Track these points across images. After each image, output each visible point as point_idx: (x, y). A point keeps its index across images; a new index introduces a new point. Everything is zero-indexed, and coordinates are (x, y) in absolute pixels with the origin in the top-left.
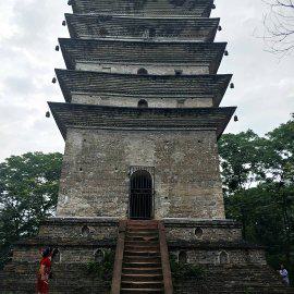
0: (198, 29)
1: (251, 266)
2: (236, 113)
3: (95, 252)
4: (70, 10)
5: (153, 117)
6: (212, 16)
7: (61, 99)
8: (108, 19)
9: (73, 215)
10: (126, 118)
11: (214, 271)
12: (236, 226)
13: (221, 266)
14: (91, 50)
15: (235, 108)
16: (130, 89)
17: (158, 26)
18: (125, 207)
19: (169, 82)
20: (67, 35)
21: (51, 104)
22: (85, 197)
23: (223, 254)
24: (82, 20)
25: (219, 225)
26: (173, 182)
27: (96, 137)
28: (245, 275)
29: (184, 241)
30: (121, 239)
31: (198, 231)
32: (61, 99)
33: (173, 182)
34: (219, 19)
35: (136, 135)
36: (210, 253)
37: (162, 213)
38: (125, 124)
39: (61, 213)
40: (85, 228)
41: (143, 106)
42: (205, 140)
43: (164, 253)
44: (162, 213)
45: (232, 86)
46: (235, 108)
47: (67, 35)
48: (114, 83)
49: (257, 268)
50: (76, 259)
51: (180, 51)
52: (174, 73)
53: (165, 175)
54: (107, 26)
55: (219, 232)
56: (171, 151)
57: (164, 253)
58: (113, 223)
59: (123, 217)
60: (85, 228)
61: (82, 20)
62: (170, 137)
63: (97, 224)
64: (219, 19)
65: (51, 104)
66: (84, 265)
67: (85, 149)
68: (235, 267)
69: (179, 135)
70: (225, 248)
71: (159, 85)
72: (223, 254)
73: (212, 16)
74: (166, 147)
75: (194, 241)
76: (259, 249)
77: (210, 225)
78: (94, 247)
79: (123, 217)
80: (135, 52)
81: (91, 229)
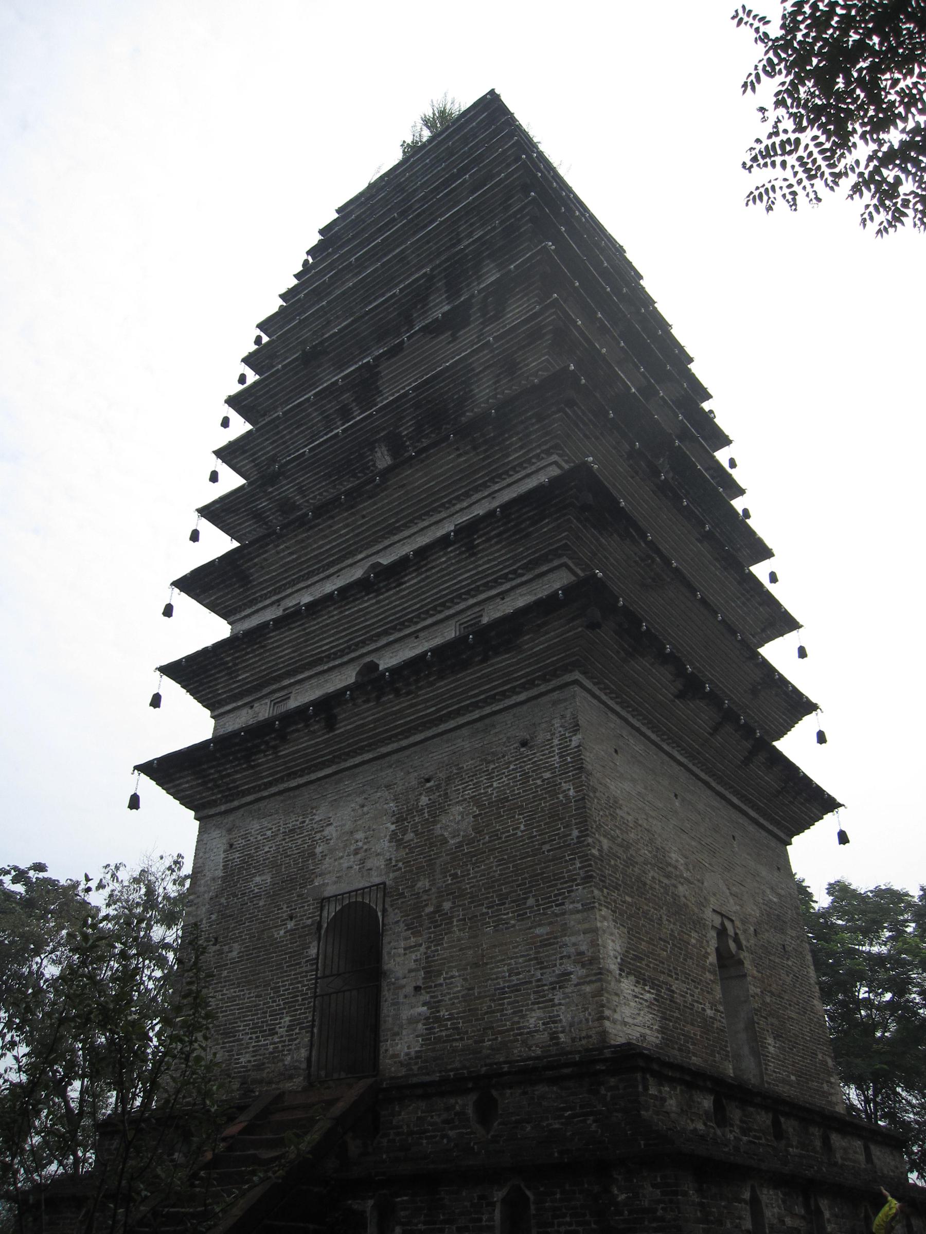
19: (412, 581)
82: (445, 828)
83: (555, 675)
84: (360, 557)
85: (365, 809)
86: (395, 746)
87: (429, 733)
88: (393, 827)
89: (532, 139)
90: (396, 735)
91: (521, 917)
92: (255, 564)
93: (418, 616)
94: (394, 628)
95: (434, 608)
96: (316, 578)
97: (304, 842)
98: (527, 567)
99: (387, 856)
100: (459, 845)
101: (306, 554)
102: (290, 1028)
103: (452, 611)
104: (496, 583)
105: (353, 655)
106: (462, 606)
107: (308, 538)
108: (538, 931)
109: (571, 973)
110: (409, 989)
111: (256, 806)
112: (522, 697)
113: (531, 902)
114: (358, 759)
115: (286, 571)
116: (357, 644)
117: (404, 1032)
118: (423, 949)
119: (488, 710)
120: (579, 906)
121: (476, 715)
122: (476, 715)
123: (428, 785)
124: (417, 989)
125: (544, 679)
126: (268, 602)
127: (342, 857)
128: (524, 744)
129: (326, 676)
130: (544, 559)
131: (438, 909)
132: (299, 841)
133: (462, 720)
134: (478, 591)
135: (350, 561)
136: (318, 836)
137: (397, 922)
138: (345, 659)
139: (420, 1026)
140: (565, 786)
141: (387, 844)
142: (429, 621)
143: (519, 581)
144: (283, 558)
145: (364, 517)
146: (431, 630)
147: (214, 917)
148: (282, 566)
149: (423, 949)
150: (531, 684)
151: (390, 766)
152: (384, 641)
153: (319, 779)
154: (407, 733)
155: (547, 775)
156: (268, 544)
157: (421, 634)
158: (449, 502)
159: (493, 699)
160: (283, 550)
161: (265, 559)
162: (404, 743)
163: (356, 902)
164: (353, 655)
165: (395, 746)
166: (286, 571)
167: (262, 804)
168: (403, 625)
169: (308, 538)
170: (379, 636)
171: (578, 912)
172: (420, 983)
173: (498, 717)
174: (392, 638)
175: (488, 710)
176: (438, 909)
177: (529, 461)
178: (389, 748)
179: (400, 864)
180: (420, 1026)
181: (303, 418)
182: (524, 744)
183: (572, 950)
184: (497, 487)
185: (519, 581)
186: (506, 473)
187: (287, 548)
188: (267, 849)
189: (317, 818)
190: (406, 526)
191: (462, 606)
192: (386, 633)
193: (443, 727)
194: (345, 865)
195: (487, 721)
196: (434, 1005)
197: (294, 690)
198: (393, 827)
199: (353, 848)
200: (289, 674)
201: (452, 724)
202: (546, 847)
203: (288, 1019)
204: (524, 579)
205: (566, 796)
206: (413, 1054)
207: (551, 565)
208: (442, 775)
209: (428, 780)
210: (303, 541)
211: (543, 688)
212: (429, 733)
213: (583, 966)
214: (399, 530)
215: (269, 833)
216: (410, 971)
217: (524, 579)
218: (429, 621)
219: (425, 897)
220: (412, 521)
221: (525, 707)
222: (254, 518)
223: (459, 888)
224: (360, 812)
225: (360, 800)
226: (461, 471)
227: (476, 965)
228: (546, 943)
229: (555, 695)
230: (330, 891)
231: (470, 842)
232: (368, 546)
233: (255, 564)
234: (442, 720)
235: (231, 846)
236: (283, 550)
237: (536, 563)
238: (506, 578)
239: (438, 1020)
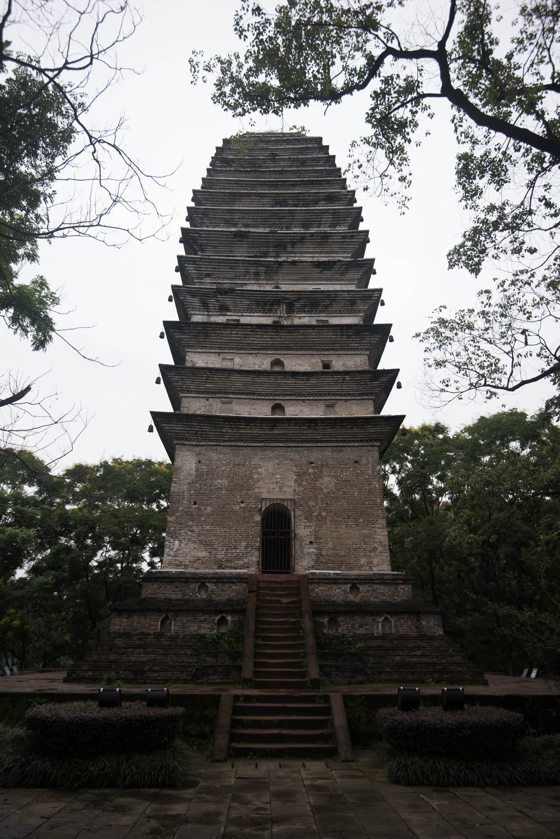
0: (353, 303)
1: (423, 637)
2: (543, 100)
3: (217, 618)
4: (178, 280)
5: (292, 430)
6: (371, 286)
7: (168, 408)
8: (230, 292)
9: (186, 566)
10: (256, 431)
11: (374, 644)
12: (406, 582)
13: (383, 637)
14: (207, 335)
15: (404, 417)
16: (260, 389)
17: (299, 299)
18: (255, 557)
19: (313, 381)
20: (175, 317)
21: (155, 415)
22: (201, 542)
23: (386, 620)
24: (193, 294)
25: (381, 579)
26: (321, 520)
27: (214, 456)
28: (413, 649)
29: (334, 603)
30: (251, 606)
31: (354, 588)
32: (168, 408)
33: (321, 520)
34: (380, 290)
35: (269, 453)
36: (368, 619)
37: (305, 563)
38: (253, 439)
39: (170, 564)
40: (203, 586)
41: (277, 369)
42: (364, 461)
43: (307, 623)
44: (305, 563)
45: (399, 386)
46: (404, 417)
47: (175, 317)
48: (238, 382)
49: (432, 638)
50: (193, 628)
51: (329, 335)
52: (319, 368)
53: (310, 512)
54: (228, 300)
55: (382, 589)
56: (318, 476)
57: (307, 623)
58: (239, 579)
59: (253, 570)
60: (203, 586)
61: (193, 294)
62: (315, 455)
63: (219, 580)
64: (380, 290)
65: (155, 415)
66: (203, 637)
67: (199, 475)
68: (401, 637)
69: (328, 453)
70: (387, 612)
71: (300, 383)
72: (386, 620)
73: (371, 286)
74: (311, 471)
75: (348, 604)
76: (433, 613)
77: (370, 580)
78: (216, 612)
79: (253, 570)
80: (268, 338)
81: (211, 586)
82: (322, 484)
83: (371, 441)
84: (270, 352)
85: (280, 466)
86: (296, 445)
87: (313, 445)
88: (296, 477)
89: (284, 135)
90: (298, 441)
91: (357, 525)
92: (216, 333)
93: (308, 395)
94: (295, 395)
95: (316, 394)
96: (243, 352)
97: (246, 471)
98: (359, 395)
99: (294, 488)
100: (329, 493)
101: (244, 340)
102: (246, 548)
103: (323, 398)
104: (345, 395)
105: (271, 398)
106: (328, 398)
107: (250, 335)
108: (364, 531)
109: (378, 548)
110: (308, 542)
111: (215, 448)
112: (356, 444)
113: (361, 520)
114: (276, 444)
115: (230, 343)
116: (275, 394)
117: (306, 557)
118: (313, 528)
119: (341, 444)
120: (381, 526)
121: (336, 444)
122: (336, 444)
123: (312, 465)
124: (311, 542)
125: (366, 441)
126: (213, 351)
127: (269, 483)
128: (356, 462)
129: (254, 401)
130: (367, 394)
131: (320, 514)
132: (244, 470)
133: (328, 444)
134: (337, 395)
135: (264, 352)
136: (254, 471)
137: (300, 515)
138: (267, 398)
139: (313, 556)
140: (374, 483)
141: (293, 484)
142: (311, 398)
143: (354, 398)
144: (232, 337)
145: (281, 338)
146: (311, 401)
147: (192, 492)
148: (229, 340)
149: (313, 528)
150: (362, 441)
151: (293, 452)
152: (288, 398)
153: (253, 446)
154: (302, 442)
155: (367, 477)
156: (228, 328)
157: (306, 402)
158: (319, 349)
159: (344, 441)
160: (234, 334)
161: (222, 334)
162: (301, 445)
163: (273, 504)
164: (271, 398)
165: (296, 445)
166: (230, 343)
167: (219, 448)
168: (299, 395)
169: (250, 335)
170: (286, 395)
171: (380, 528)
172: (312, 540)
173: (343, 448)
174: (293, 398)
175: (341, 444)
176: (320, 514)
177: (358, 349)
178: (293, 445)
179: (300, 493)
180: (313, 556)
181: (235, 266)
182: (356, 462)
183: (378, 540)
184: (342, 352)
185: (354, 398)
186: (347, 349)
187: (237, 334)
188: (223, 469)
189: (253, 463)
190: (296, 349)
191: (328, 398)
192: (290, 395)
193: (319, 444)
194: (271, 487)
195: (339, 448)
196: (320, 549)
197: (235, 401)
198: (296, 477)
199: (275, 480)
200: (234, 393)
201: (324, 444)
202: (367, 503)
203: (244, 544)
204: (357, 398)
205: (375, 487)
206: (310, 566)
207: (369, 397)
208: (319, 463)
209: (312, 463)
210: (246, 334)
211: (365, 444)
212: (313, 445)
213: (382, 546)
214: (292, 349)
215: (224, 462)
216: (307, 535)
217: (357, 398)
218: (311, 398)
219: (313, 509)
220: (300, 349)
221: (356, 448)
222: (202, 303)
223: (330, 509)
224: (277, 466)
225: (277, 461)
226: (331, 341)
227: (338, 538)
228: (367, 536)
229: (369, 448)
230: (264, 496)
231: (334, 493)
232: (276, 350)
233: (216, 333)
234: (320, 442)
235: (200, 462)
236: (234, 334)
237: (363, 394)
238: (350, 395)
239: (321, 555)
